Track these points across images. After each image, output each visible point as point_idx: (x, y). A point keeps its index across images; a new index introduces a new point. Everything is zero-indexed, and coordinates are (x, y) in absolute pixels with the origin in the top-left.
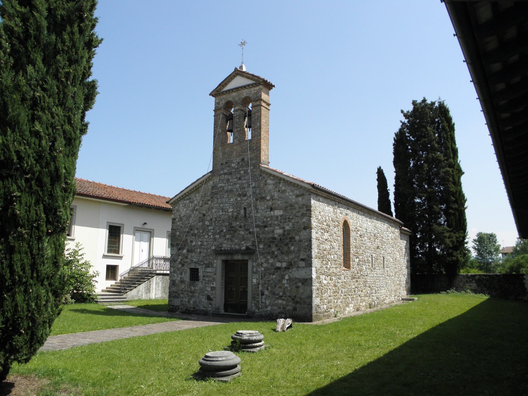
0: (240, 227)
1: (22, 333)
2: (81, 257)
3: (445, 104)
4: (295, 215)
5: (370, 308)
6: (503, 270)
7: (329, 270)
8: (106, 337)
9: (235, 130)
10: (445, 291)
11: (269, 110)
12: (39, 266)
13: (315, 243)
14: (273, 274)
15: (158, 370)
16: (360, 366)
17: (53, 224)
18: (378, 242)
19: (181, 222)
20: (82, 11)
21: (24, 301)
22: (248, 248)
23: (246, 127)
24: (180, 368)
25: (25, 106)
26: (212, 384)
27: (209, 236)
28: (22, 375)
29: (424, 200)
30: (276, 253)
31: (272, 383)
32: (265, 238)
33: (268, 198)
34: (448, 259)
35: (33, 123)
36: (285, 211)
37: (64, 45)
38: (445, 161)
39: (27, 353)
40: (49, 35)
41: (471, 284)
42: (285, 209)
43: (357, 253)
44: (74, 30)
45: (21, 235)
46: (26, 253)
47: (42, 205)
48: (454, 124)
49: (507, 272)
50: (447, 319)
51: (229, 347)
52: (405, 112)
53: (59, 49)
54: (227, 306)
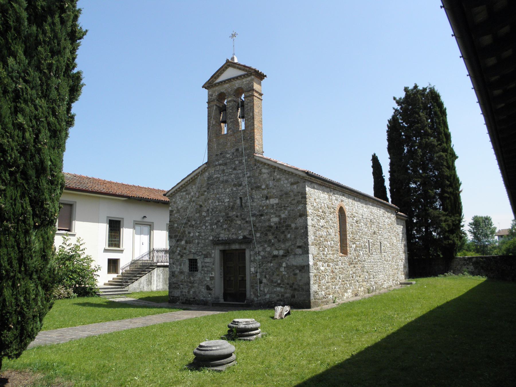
0: (237, 217)
1: (11, 328)
2: (82, 252)
3: (436, 89)
4: (290, 203)
5: (368, 293)
6: (499, 252)
7: (326, 256)
8: (105, 329)
9: (228, 121)
10: (443, 274)
11: (262, 100)
12: (26, 259)
13: (311, 231)
14: (271, 263)
15: (154, 361)
16: (358, 351)
17: (40, 217)
18: (374, 228)
19: (178, 214)
20: (62, 2)
21: (12, 295)
22: (245, 237)
23: (240, 117)
24: (176, 358)
25: (7, 98)
26: (206, 374)
27: (206, 226)
28: (16, 370)
29: (419, 185)
30: (273, 241)
31: (267, 372)
32: (262, 227)
33: (263, 187)
34: (445, 242)
35: (16, 115)
36: (280, 199)
37: (45, 35)
38: (439, 146)
39: (17, 348)
40: (30, 26)
41: (468, 267)
42: (280, 197)
43: (354, 239)
44: (55, 21)
45: (7, 229)
46: (13, 247)
47: (27, 198)
48: (445, 109)
49: (503, 254)
50: (445, 301)
51: (226, 335)
52: (398, 99)
53: (40, 40)
54: (226, 295)
